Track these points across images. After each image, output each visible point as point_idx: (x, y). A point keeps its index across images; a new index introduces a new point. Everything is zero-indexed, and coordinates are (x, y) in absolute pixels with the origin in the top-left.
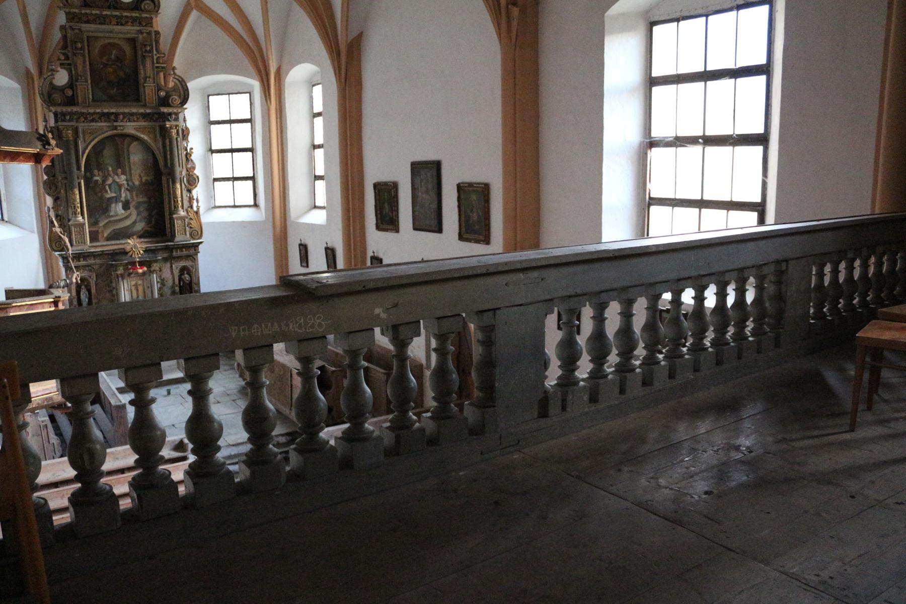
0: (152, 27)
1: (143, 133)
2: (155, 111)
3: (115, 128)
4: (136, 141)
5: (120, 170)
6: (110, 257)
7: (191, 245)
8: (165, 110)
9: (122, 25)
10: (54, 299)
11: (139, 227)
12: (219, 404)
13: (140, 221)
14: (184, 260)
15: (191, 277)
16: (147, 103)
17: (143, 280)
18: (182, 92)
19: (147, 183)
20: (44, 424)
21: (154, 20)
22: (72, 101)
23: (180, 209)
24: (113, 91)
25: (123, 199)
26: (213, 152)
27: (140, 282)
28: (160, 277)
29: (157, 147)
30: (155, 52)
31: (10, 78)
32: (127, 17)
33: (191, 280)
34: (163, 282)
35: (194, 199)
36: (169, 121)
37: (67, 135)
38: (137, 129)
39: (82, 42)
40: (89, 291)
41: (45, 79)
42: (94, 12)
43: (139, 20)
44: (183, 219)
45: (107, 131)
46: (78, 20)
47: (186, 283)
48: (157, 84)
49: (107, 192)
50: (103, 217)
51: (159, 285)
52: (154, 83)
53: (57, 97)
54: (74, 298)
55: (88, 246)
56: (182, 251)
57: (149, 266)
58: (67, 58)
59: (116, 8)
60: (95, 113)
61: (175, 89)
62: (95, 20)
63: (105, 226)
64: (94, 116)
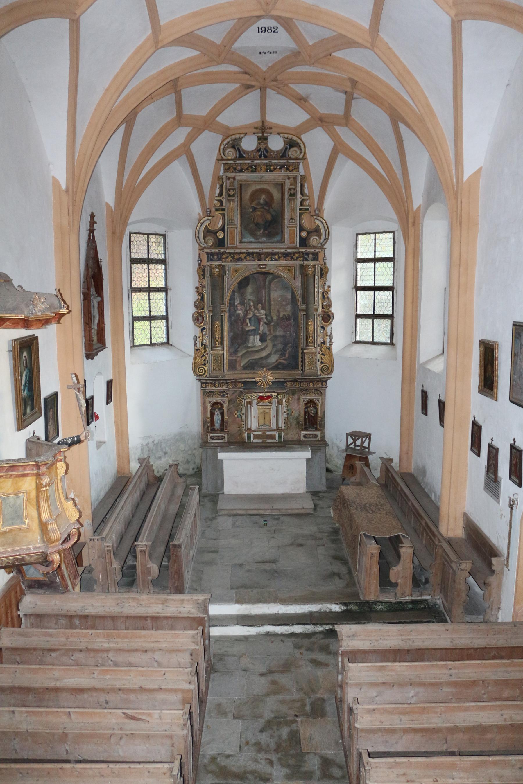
0: (299, 171)
5: (260, 305)
13: (275, 353)
40: (222, 414)
48: (300, 225)
49: (247, 324)
51: (285, 415)
63: (243, 356)
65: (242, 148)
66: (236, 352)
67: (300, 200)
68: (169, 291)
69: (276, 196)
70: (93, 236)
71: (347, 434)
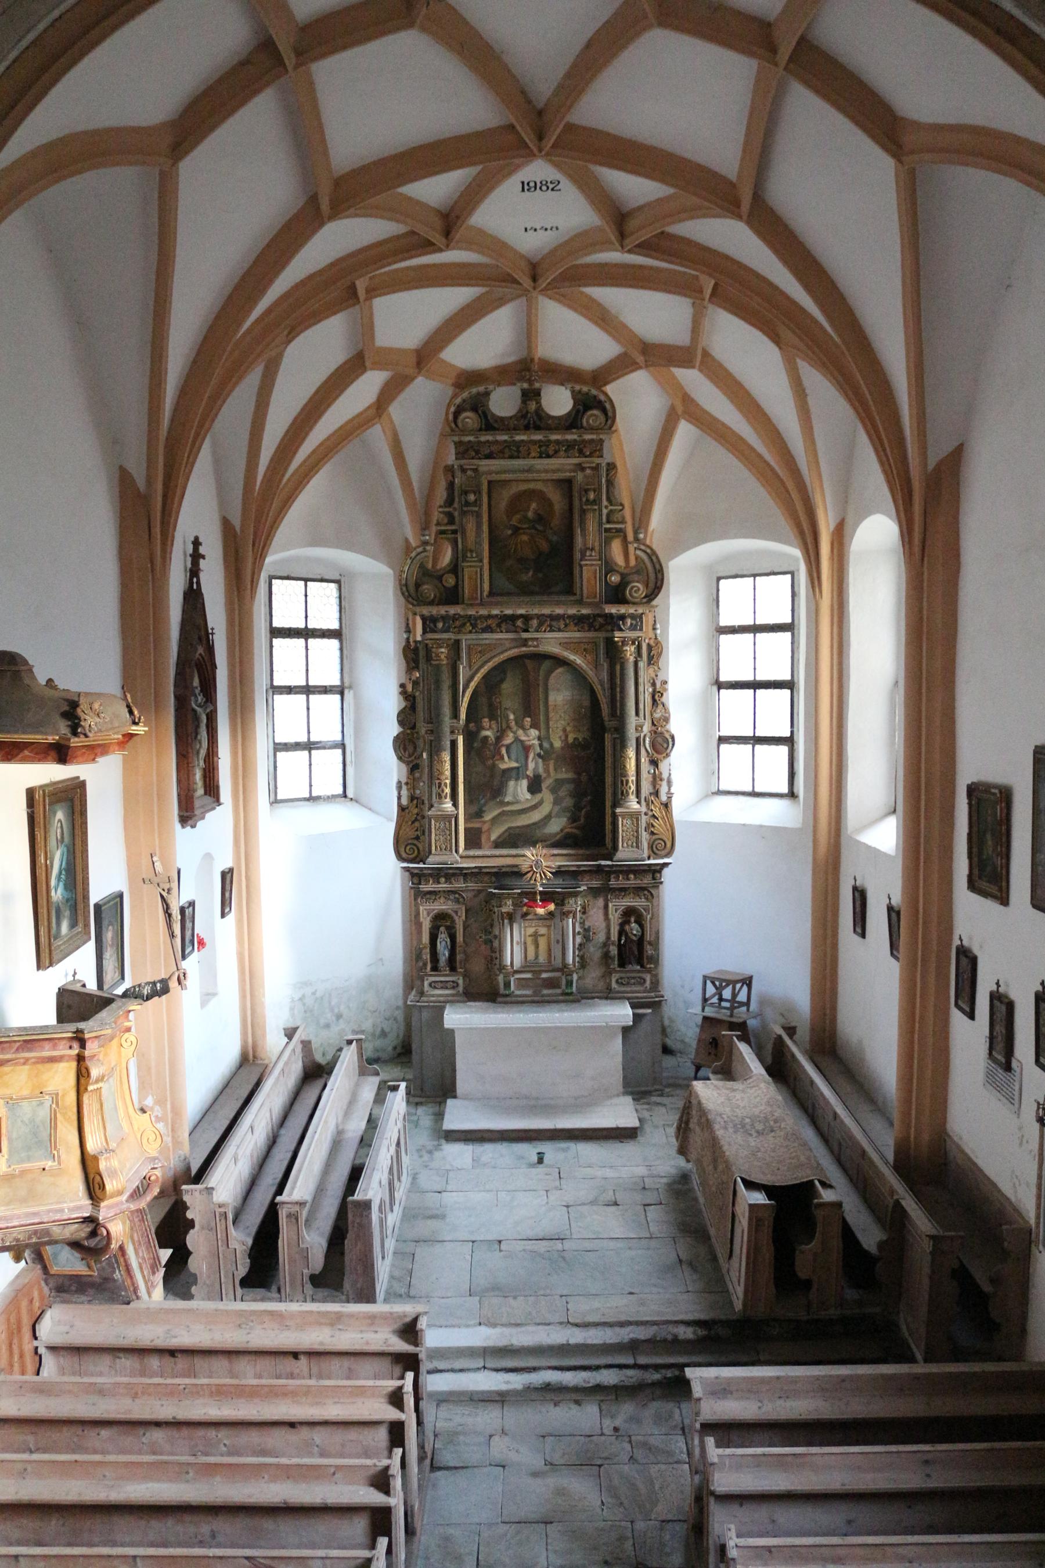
1: (575, 651)
2: (597, 612)
3: (525, 642)
4: (560, 666)
5: (529, 719)
6: (494, 879)
7: (646, 868)
8: (613, 610)
9: (548, 456)
10: (74, 1033)
11: (556, 827)
12: (613, 1208)
13: (558, 816)
14: (632, 895)
15: (641, 926)
16: (585, 595)
17: (549, 927)
18: (652, 576)
19: (576, 745)
20: (222, 1210)
21: (606, 445)
22: (452, 596)
23: (633, 798)
24: (528, 576)
25: (530, 773)
26: (720, 685)
27: (543, 931)
28: (582, 923)
29: (598, 677)
30: (605, 503)
31: (373, 557)
32: (557, 442)
33: (643, 934)
34: (587, 934)
35: (661, 780)
36: (621, 630)
37: (437, 655)
38: (566, 645)
39: (478, 492)
40: (453, 937)
41: (413, 560)
44: (635, 816)
45: (510, 649)
46: (473, 454)
47: (632, 941)
48: (607, 563)
49: (502, 758)
50: (491, 804)
51: (579, 940)
52: (600, 559)
53: (429, 590)
54: (425, 947)
55: (460, 857)
56: (628, 879)
57: (560, 903)
58: (451, 521)
59: (537, 428)
60: (490, 616)
61: (639, 570)
62: (502, 452)
63: (494, 820)
64: (490, 622)
66: (479, 814)
67: (605, 511)
68: (346, 692)
70: (198, 583)
71: (705, 978)
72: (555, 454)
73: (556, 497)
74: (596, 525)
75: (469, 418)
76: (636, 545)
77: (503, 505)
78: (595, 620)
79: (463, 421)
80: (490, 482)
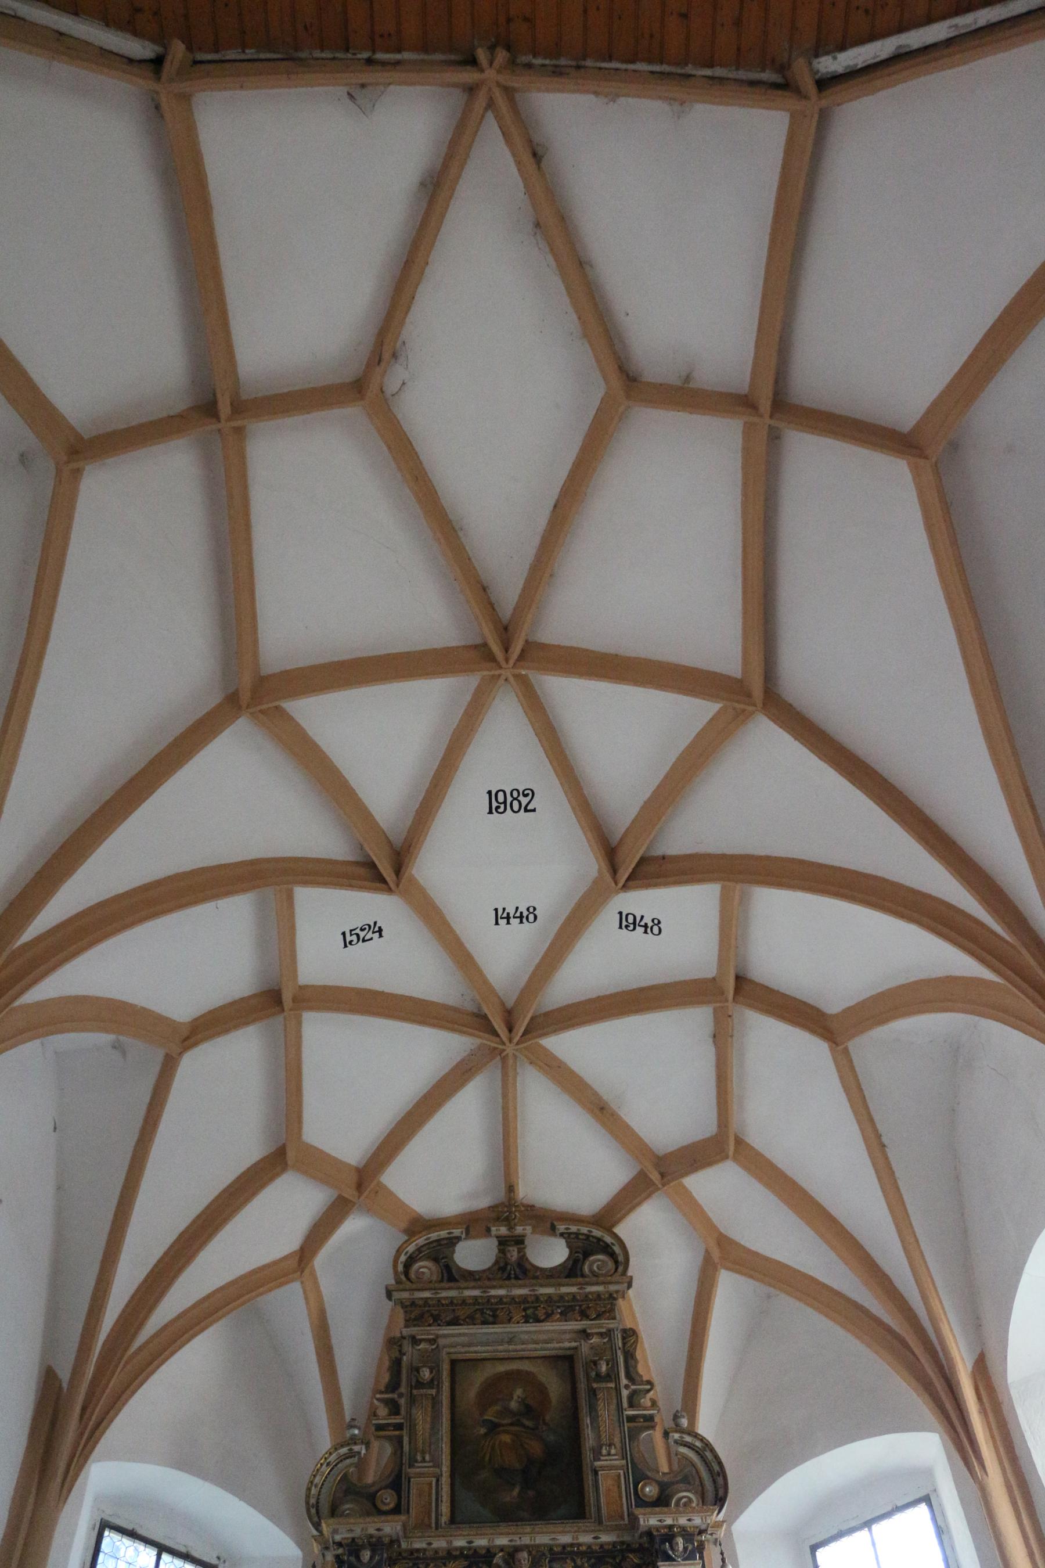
8: (650, 1520)
9: (538, 1321)
30: (624, 1381)
31: (272, 1517)
32: (549, 1298)
39: (435, 1369)
42: (467, 1293)
43: (580, 1306)
58: (394, 1408)
65: (455, 1262)
67: (625, 1393)
69: (555, 1386)
72: (548, 1317)
73: (555, 1386)
74: (613, 1407)
75: (425, 1268)
76: (677, 1436)
77: (472, 1393)
78: (624, 1558)
79: (417, 1271)
80: (453, 1363)
